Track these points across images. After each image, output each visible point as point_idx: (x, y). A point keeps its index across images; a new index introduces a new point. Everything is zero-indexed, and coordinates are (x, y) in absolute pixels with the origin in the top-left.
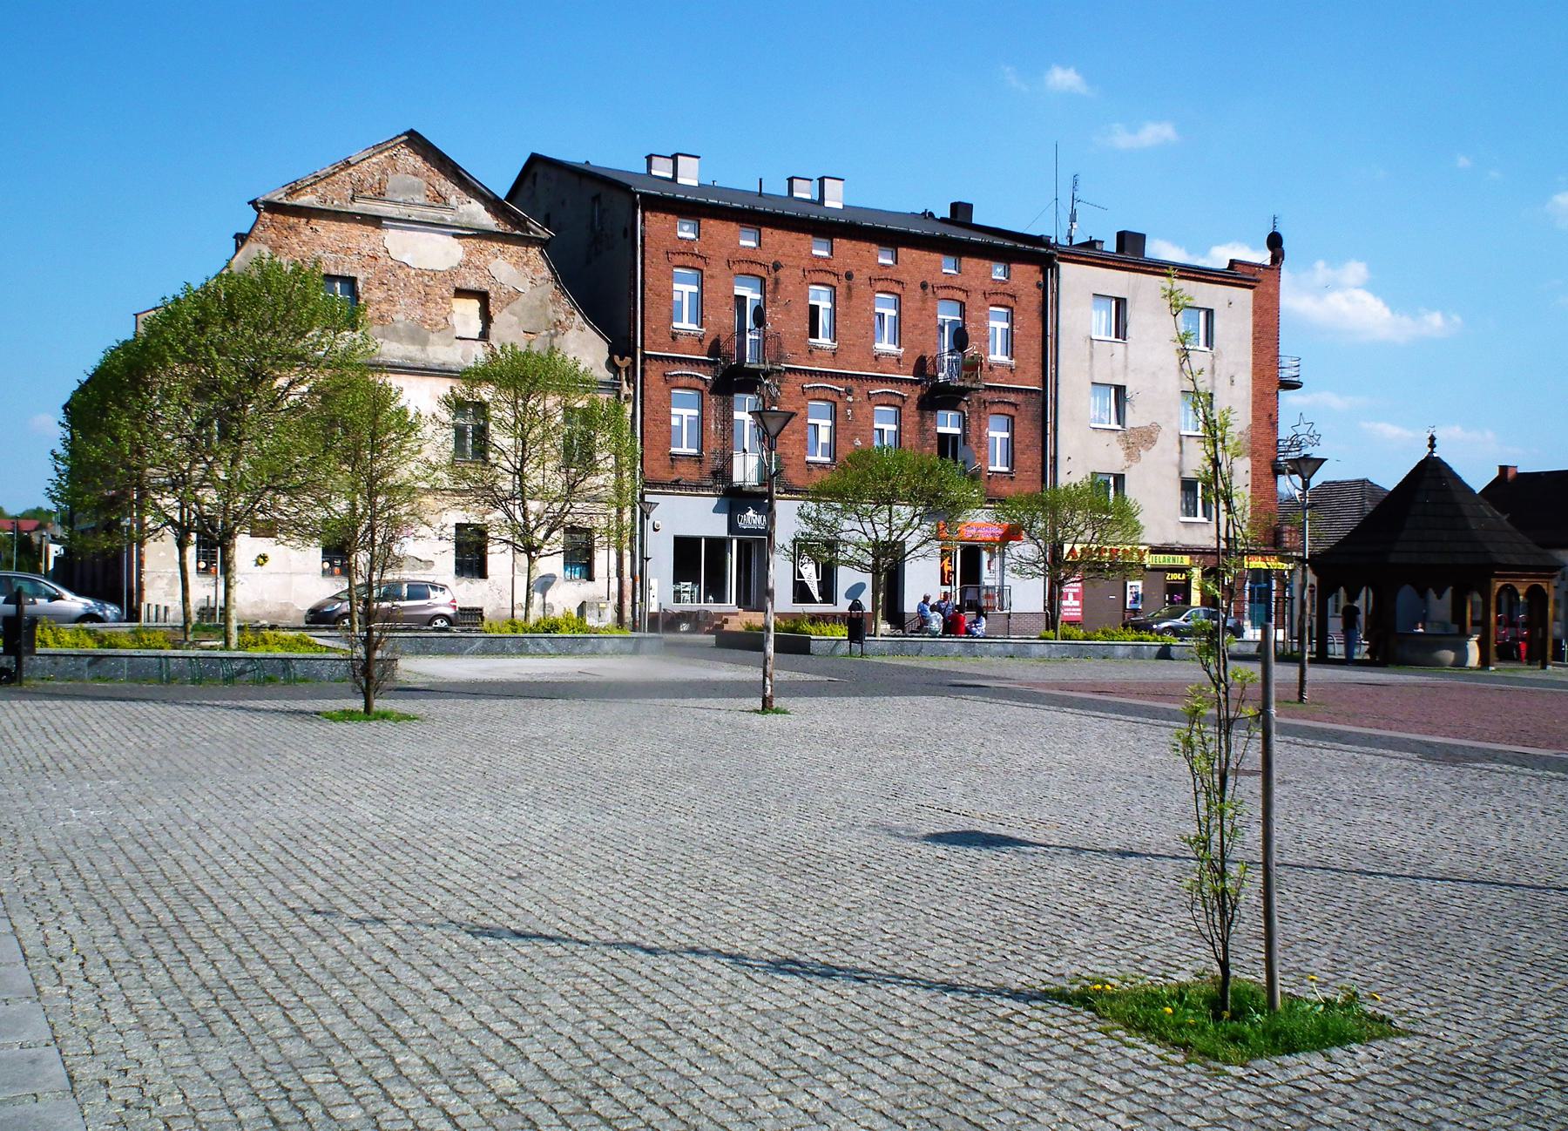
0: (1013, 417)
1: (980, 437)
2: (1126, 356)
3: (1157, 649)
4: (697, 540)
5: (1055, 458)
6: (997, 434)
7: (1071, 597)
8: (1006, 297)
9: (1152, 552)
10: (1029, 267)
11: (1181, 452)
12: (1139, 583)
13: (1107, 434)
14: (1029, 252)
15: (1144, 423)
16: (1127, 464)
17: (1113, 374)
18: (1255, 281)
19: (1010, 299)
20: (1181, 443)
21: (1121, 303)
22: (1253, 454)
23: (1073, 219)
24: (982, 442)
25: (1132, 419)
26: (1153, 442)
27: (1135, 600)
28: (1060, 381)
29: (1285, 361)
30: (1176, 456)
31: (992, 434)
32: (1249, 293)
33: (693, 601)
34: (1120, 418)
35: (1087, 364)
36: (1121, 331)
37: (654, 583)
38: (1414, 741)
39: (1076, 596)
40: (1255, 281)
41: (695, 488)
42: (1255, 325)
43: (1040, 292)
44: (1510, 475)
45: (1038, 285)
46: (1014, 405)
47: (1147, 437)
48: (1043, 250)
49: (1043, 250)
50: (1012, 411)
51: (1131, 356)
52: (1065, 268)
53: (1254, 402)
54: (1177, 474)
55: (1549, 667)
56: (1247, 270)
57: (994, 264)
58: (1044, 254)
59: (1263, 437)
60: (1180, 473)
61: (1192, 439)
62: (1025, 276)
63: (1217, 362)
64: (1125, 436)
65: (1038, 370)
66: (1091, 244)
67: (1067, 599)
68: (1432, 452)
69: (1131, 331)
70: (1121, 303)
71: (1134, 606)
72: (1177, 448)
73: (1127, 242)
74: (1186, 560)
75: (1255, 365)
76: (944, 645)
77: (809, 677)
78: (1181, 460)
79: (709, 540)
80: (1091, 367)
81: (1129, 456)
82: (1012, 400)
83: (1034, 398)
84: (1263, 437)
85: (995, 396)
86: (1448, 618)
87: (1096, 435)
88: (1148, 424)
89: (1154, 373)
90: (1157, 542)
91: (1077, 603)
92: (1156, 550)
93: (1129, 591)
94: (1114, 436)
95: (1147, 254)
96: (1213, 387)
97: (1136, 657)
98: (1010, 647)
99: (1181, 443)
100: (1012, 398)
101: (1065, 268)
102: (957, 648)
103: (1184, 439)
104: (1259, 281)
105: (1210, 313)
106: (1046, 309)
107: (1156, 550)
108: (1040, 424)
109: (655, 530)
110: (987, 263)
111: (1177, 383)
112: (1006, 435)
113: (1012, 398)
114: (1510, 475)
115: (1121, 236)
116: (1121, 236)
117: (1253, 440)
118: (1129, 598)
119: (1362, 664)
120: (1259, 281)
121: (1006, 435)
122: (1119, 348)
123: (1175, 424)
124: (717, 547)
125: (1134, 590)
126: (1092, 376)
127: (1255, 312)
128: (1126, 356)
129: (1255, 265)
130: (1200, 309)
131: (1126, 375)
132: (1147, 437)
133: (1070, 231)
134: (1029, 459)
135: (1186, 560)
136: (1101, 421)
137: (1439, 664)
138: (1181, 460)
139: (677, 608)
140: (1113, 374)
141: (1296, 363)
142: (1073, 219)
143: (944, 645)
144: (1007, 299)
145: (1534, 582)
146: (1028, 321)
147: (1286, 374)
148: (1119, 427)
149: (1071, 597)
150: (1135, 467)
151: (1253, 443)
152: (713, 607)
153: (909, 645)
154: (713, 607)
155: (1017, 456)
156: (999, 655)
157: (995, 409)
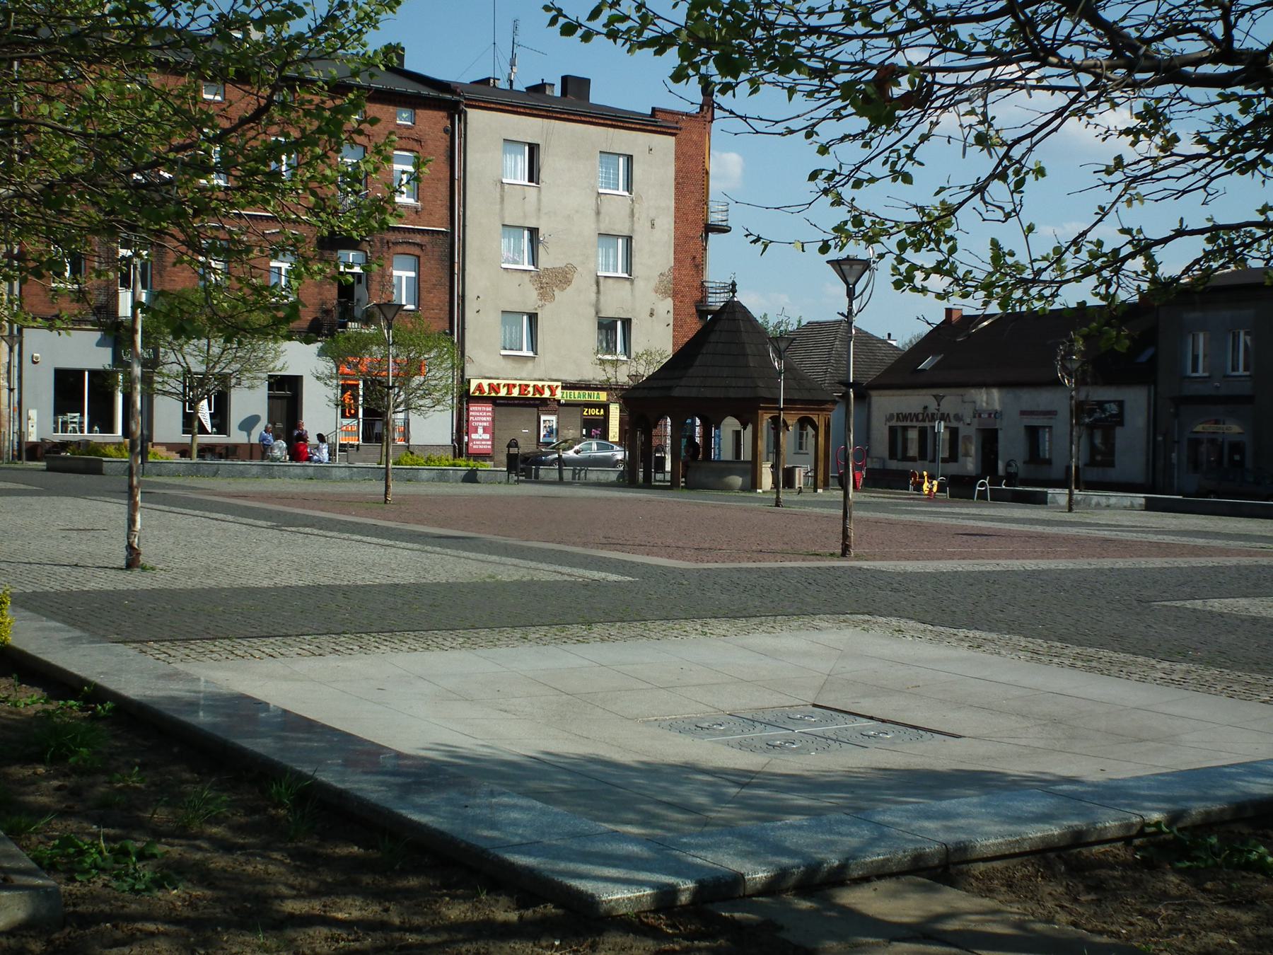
0: (419, 257)
1: (383, 276)
2: (539, 200)
3: (463, 473)
4: (80, 373)
5: (462, 298)
6: (403, 275)
7: (480, 431)
8: (411, 141)
9: (563, 388)
10: (436, 113)
11: (598, 292)
12: (554, 418)
13: (519, 274)
14: (434, 99)
15: (559, 264)
16: (540, 303)
17: (525, 217)
18: (677, 128)
19: (415, 143)
20: (598, 284)
21: (533, 149)
22: (675, 295)
23: (512, 64)
24: (387, 282)
25: (545, 260)
26: (569, 282)
27: (550, 433)
28: (467, 224)
29: (713, 206)
30: (593, 296)
31: (396, 273)
32: (671, 141)
33: (80, 429)
34: (534, 259)
35: (498, 207)
36: (533, 175)
37: (33, 413)
38: (351, 522)
39: (485, 430)
40: (677, 128)
41: (77, 322)
42: (678, 171)
43: (447, 137)
44: (955, 317)
45: (446, 131)
46: (420, 246)
47: (562, 277)
48: (449, 96)
49: (449, 96)
50: (417, 251)
51: (544, 199)
52: (474, 115)
53: (676, 246)
54: (593, 312)
55: (820, 491)
56: (669, 117)
57: (399, 109)
58: (450, 101)
59: (687, 279)
60: (597, 313)
61: (610, 281)
62: (432, 122)
63: (637, 206)
64: (539, 276)
65: (446, 212)
66: (539, 89)
67: (476, 432)
68: (734, 296)
69: (544, 175)
70: (533, 149)
71: (548, 440)
72: (594, 288)
73: (570, 87)
74: (603, 396)
75: (677, 209)
76: (241, 468)
77: (1216, 604)
78: (598, 300)
79: (93, 373)
80: (502, 209)
81: (543, 296)
82: (418, 241)
83: (441, 240)
84: (687, 279)
85: (400, 237)
86: (886, 454)
87: (506, 275)
88: (563, 266)
89: (569, 216)
90: (572, 378)
91: (487, 436)
92: (567, 386)
93: (542, 425)
94: (526, 277)
95: (593, 99)
96: (633, 230)
97: (440, 480)
98: (310, 471)
99: (598, 284)
100: (418, 239)
101: (474, 115)
102: (255, 470)
103: (601, 280)
104: (680, 129)
105: (630, 159)
106: (454, 154)
107: (567, 386)
108: (447, 264)
109: (35, 363)
110: (391, 109)
111: (593, 226)
112: (413, 274)
113: (418, 239)
114: (955, 317)
115: (565, 80)
116: (565, 80)
117: (676, 281)
118: (542, 434)
119: (569, 484)
120: (680, 129)
121: (413, 274)
122: (532, 192)
123: (592, 265)
124: (102, 381)
125: (548, 424)
126: (502, 217)
127: (677, 158)
128: (539, 200)
129: (678, 113)
130: (620, 155)
131: (539, 218)
132: (562, 277)
133: (510, 75)
134: (437, 298)
135: (603, 396)
136: (515, 262)
137: (728, 488)
138: (598, 300)
139: (60, 437)
140: (525, 217)
141: (724, 208)
142: (512, 64)
143: (241, 468)
144: (414, 142)
145: (804, 414)
146: (435, 169)
147: (714, 218)
148: (532, 268)
149: (480, 431)
150: (549, 306)
151: (675, 284)
152: (98, 437)
153: (205, 467)
154: (98, 437)
155: (424, 294)
156: (298, 476)
157: (399, 249)
